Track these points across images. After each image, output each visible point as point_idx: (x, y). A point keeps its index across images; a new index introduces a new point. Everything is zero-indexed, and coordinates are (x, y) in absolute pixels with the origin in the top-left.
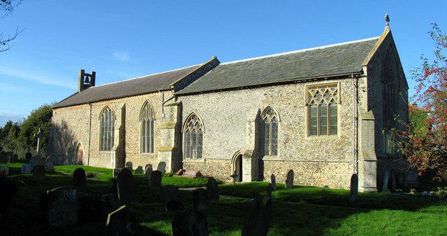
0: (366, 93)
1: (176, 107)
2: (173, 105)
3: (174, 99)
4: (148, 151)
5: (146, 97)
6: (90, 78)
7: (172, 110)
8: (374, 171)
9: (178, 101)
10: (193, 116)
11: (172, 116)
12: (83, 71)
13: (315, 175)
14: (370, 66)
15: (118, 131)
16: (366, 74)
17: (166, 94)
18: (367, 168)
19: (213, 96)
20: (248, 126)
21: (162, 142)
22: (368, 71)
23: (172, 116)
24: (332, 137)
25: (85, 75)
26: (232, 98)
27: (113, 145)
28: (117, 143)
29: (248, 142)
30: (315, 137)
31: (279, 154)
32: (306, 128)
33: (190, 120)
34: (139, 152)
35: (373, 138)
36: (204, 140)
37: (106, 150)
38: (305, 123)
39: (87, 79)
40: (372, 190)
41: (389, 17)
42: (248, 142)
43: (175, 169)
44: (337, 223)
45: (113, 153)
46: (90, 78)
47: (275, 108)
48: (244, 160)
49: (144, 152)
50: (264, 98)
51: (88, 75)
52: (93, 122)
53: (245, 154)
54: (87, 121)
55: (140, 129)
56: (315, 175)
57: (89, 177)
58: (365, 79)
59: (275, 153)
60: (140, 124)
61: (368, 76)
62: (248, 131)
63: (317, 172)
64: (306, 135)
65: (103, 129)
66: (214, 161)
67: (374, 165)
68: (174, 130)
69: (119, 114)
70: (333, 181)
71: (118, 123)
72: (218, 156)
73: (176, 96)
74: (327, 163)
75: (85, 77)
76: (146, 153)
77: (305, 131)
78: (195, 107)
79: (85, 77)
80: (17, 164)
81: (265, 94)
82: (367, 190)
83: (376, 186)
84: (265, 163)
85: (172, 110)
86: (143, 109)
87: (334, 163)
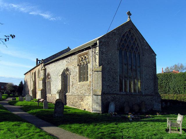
8: (100, 101)
12: (37, 59)
14: (103, 40)
16: (98, 45)
18: (95, 99)
22: (99, 43)
25: (39, 61)
30: (82, 83)
35: (101, 82)
40: (98, 112)
43: (129, 92)
47: (69, 67)
51: (40, 61)
58: (98, 48)
61: (99, 46)
67: (100, 97)
73: (45, 65)
75: (39, 62)
79: (39, 62)
82: (95, 112)
83: (101, 110)
84: (67, 96)
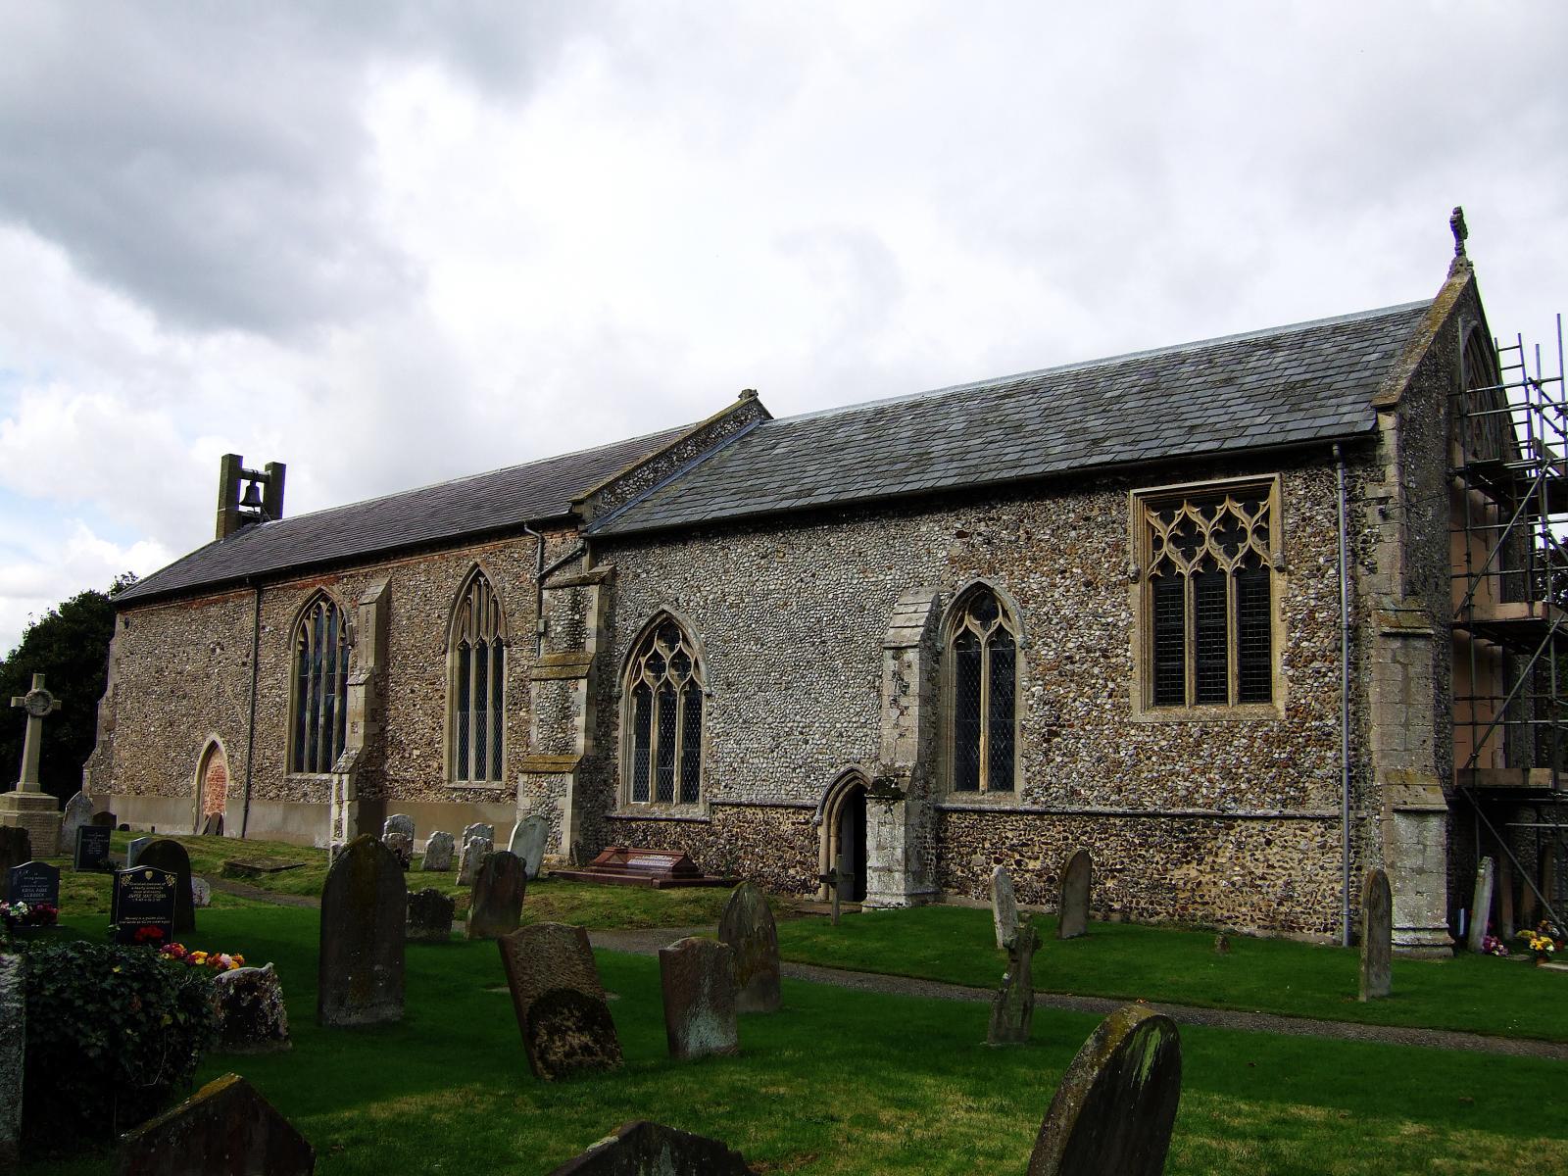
0: (1395, 524)
1: (593, 592)
2: (586, 582)
3: (585, 560)
4: (480, 775)
5: (475, 554)
6: (260, 485)
7: (576, 606)
9: (603, 568)
10: (667, 628)
11: (576, 629)
12: (232, 466)
13: (1177, 875)
15: (361, 691)
17: (554, 541)
19: (743, 551)
20: (890, 665)
21: (535, 734)
23: (576, 629)
24: (1257, 710)
25: (245, 475)
26: (823, 554)
27: (341, 747)
28: (355, 740)
29: (888, 733)
31: (1020, 785)
32: (1136, 673)
33: (648, 644)
34: (445, 775)
36: (710, 725)
37: (313, 770)
38: (1135, 651)
39: (252, 490)
41: (1468, 220)
42: (888, 733)
44: (1401, 1118)
45: (340, 782)
46: (260, 485)
48: (874, 811)
49: (464, 775)
50: (958, 548)
51: (254, 477)
52: (267, 658)
53: (879, 785)
54: (238, 654)
55: (448, 682)
56: (1177, 875)
57: (116, 851)
59: (1003, 780)
60: (451, 660)
62: (889, 688)
63: (1185, 858)
64: (1136, 698)
65: (303, 683)
66: (749, 812)
68: (583, 684)
69: (364, 618)
70: (1255, 898)
71: (363, 663)
72: (762, 793)
74: (1229, 821)
75: (245, 484)
76: (1194, 713)
77: (1137, 688)
78: (671, 588)
79: (245, 484)
80: (338, 725)
81: (960, 535)
85: (576, 606)
86: (462, 601)
87: (1258, 825)
